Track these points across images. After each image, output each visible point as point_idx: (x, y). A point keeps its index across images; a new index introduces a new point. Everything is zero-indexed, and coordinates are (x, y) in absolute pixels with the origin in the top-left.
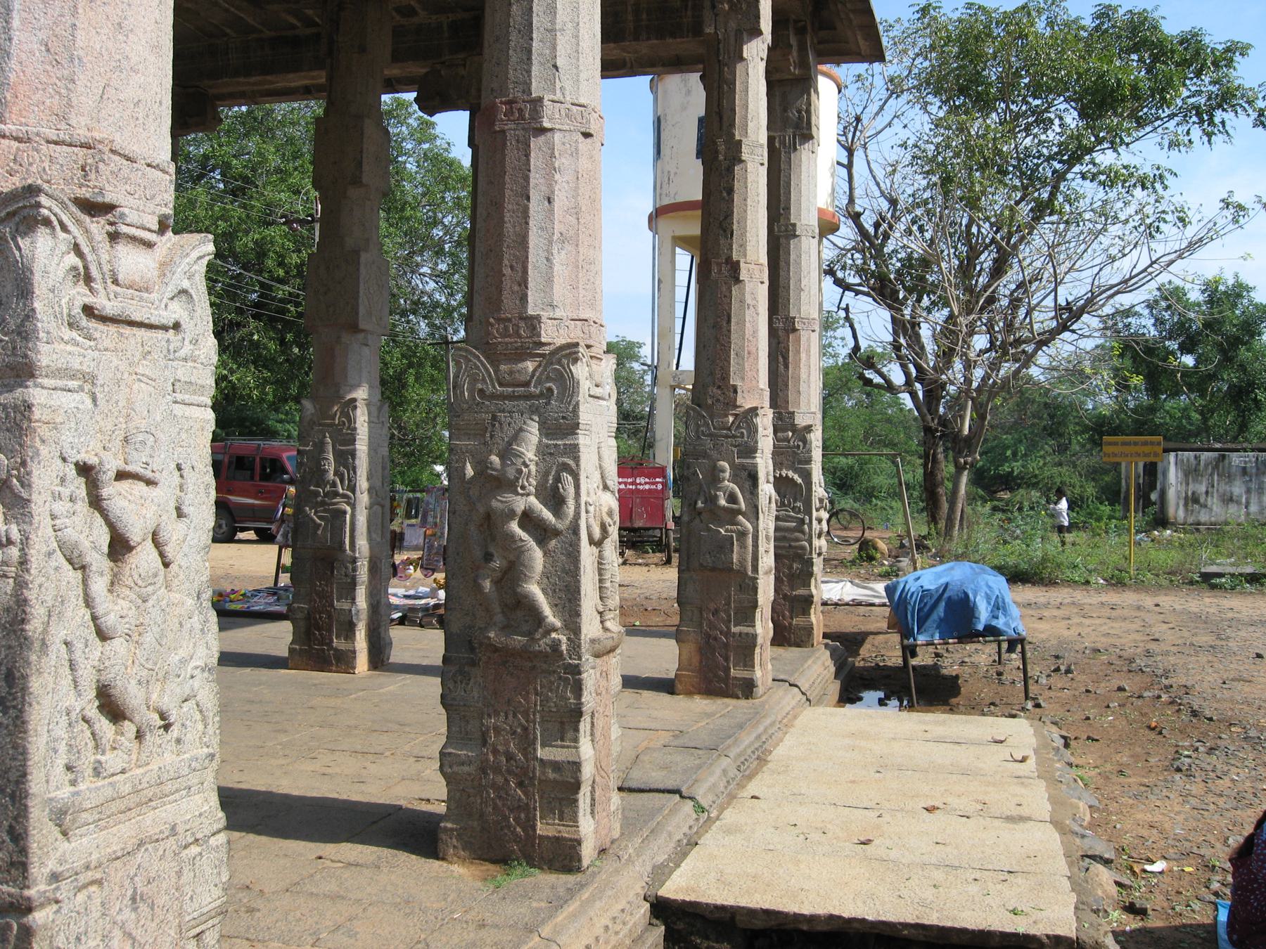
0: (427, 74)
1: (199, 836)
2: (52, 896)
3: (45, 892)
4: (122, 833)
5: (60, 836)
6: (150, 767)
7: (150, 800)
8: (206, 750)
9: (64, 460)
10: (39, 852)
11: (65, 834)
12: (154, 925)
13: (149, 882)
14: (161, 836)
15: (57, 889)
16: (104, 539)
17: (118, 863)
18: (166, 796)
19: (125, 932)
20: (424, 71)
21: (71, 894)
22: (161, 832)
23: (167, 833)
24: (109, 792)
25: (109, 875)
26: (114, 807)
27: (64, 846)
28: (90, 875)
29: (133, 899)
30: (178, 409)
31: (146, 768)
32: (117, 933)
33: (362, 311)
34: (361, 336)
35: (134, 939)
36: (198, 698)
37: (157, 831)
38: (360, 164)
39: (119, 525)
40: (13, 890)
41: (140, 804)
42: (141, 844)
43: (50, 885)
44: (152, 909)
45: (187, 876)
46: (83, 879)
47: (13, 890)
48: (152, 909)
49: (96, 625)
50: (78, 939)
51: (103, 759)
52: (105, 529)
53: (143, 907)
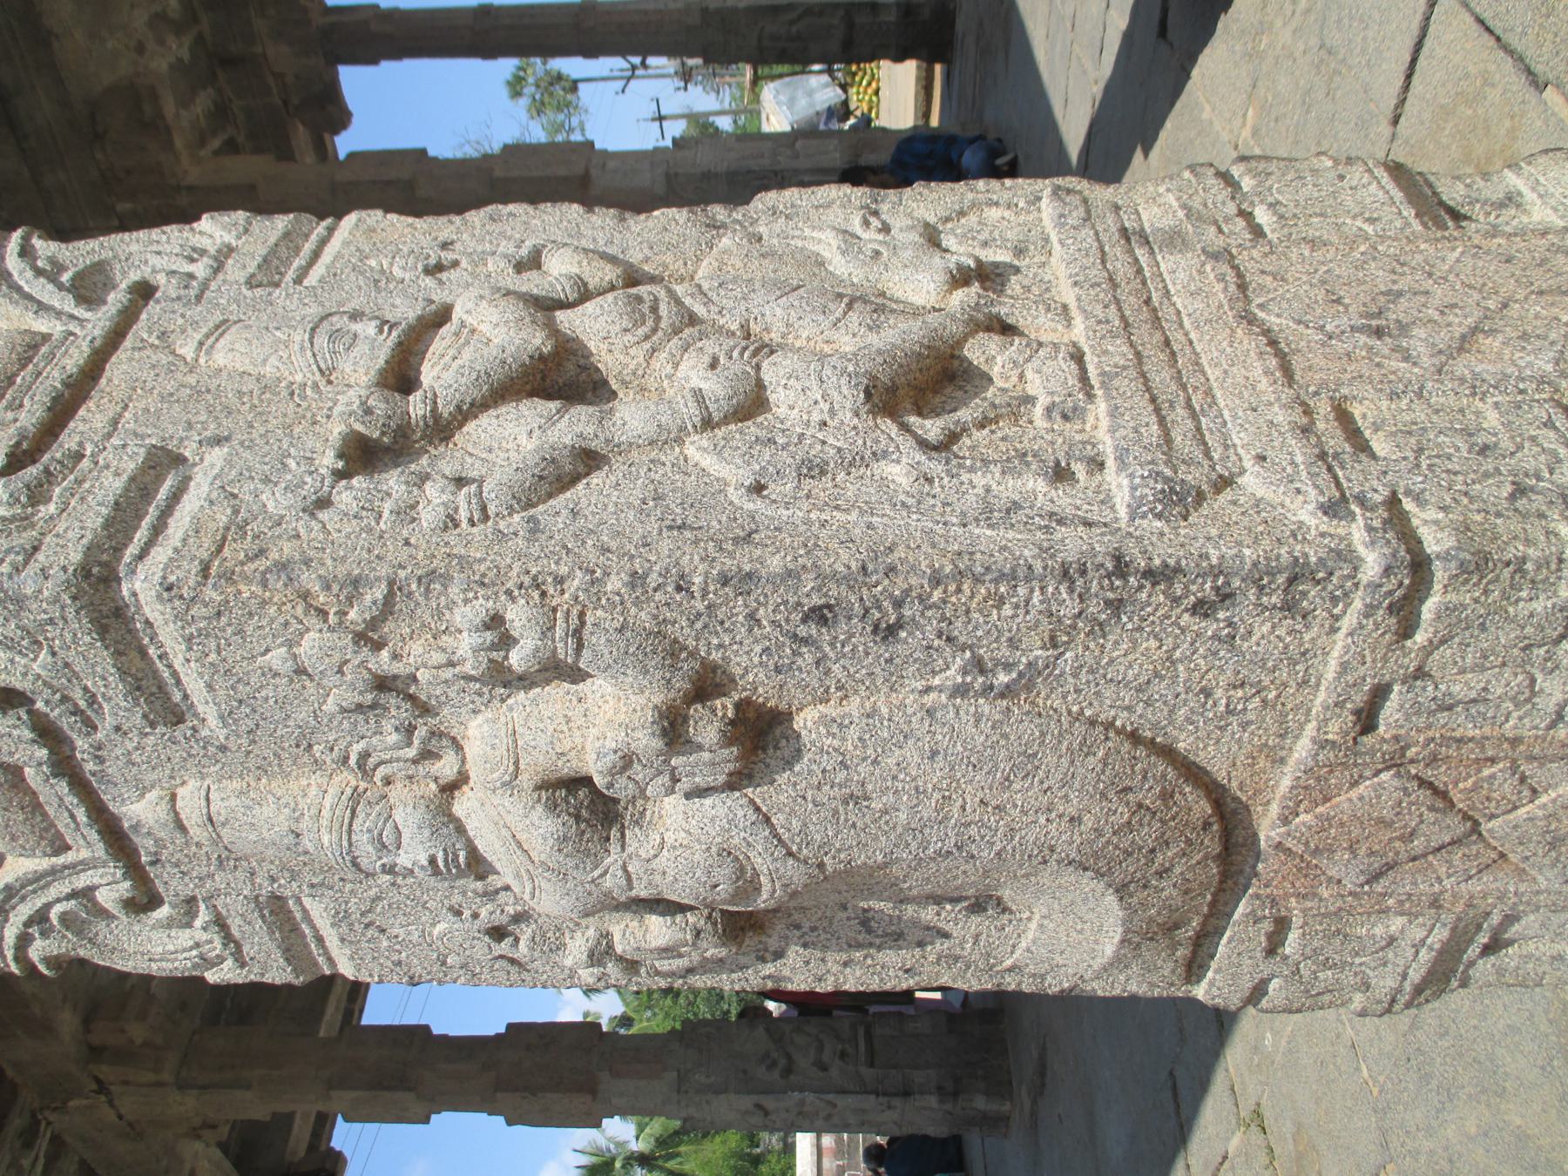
0: (303, 123)
1: (1231, 209)
2: (1382, 513)
3: (1370, 529)
4: (1232, 371)
5: (1228, 494)
6: (1073, 305)
7: (1148, 302)
8: (1045, 202)
9: (324, 503)
10: (1266, 543)
11: (1224, 483)
12: (1438, 291)
13: (1338, 301)
14: (1231, 276)
15: (1361, 500)
16: (533, 411)
17: (1297, 363)
18: (1140, 271)
19: (1461, 349)
20: (301, 128)
21: (1375, 468)
22: (1221, 278)
23: (1225, 268)
24: (1126, 384)
25: (1323, 384)
26: (1161, 377)
27: (1252, 482)
28: (1325, 423)
29: (1379, 333)
30: (312, 279)
31: (1074, 312)
32: (1461, 366)
33: (562, 171)
34: (594, 172)
35: (1475, 330)
36: (932, 219)
37: (1219, 287)
38: (389, 183)
39: (498, 375)
40: (1358, 604)
41: (1156, 321)
42: (1249, 319)
43: (1352, 515)
44: (1400, 294)
45: (1318, 228)
46: (1335, 441)
47: (1358, 604)
48: (1400, 294)
49: (726, 420)
50: (1484, 450)
51: (1043, 401)
52: (507, 410)
53: (1399, 311)
